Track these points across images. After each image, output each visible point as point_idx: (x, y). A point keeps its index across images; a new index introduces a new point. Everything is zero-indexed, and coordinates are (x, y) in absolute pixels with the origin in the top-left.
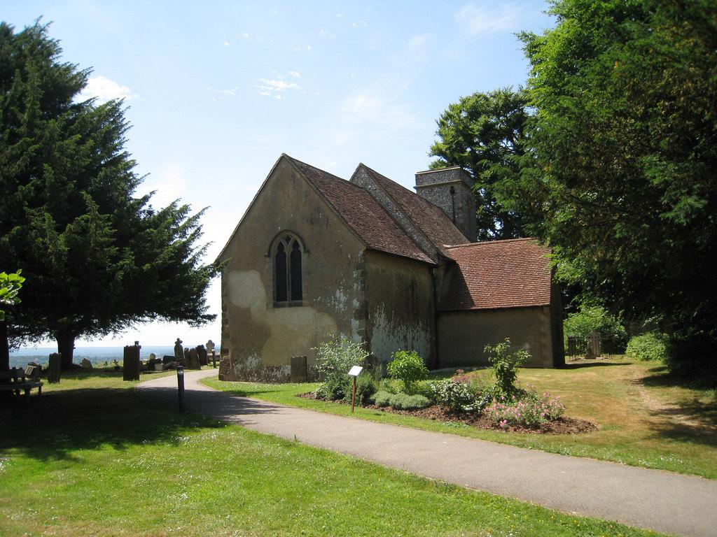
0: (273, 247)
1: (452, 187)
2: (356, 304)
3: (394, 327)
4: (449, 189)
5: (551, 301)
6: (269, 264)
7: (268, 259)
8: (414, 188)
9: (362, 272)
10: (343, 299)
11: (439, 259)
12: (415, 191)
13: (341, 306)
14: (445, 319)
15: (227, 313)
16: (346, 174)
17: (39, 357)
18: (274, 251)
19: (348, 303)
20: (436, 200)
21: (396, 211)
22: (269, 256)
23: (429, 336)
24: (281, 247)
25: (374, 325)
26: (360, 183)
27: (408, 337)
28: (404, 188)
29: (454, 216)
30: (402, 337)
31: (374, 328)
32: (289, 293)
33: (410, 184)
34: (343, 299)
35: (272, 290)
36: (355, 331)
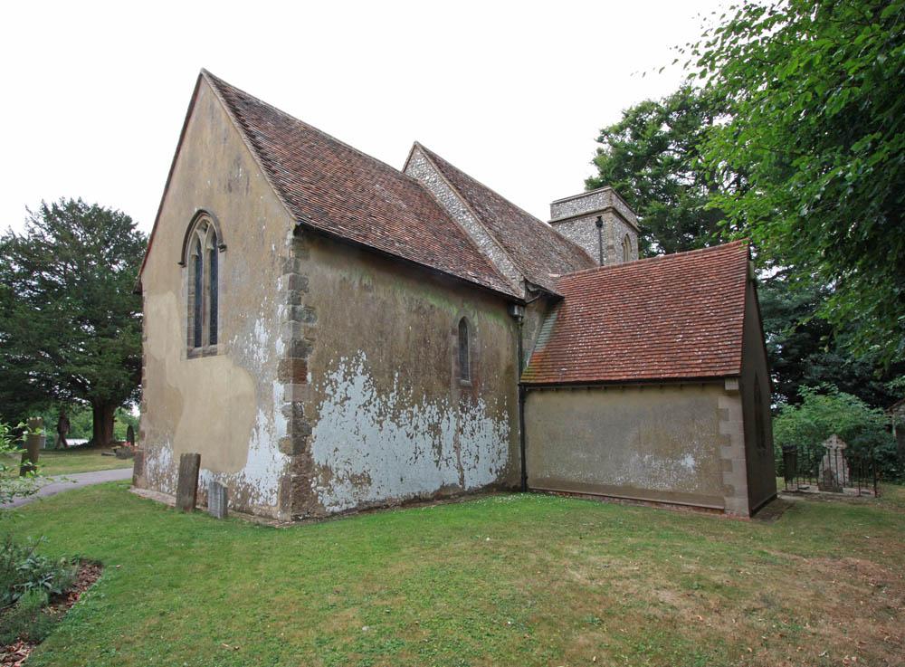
1: (599, 218)
2: (281, 348)
3: (400, 406)
4: (595, 219)
7: (184, 270)
10: (263, 338)
11: (528, 290)
13: (261, 352)
14: (536, 400)
16: (396, 159)
19: (270, 346)
20: (578, 238)
21: (464, 213)
23: (504, 427)
25: (321, 397)
26: (413, 173)
27: (444, 426)
29: (602, 260)
30: (423, 427)
33: (544, 216)
35: (186, 314)
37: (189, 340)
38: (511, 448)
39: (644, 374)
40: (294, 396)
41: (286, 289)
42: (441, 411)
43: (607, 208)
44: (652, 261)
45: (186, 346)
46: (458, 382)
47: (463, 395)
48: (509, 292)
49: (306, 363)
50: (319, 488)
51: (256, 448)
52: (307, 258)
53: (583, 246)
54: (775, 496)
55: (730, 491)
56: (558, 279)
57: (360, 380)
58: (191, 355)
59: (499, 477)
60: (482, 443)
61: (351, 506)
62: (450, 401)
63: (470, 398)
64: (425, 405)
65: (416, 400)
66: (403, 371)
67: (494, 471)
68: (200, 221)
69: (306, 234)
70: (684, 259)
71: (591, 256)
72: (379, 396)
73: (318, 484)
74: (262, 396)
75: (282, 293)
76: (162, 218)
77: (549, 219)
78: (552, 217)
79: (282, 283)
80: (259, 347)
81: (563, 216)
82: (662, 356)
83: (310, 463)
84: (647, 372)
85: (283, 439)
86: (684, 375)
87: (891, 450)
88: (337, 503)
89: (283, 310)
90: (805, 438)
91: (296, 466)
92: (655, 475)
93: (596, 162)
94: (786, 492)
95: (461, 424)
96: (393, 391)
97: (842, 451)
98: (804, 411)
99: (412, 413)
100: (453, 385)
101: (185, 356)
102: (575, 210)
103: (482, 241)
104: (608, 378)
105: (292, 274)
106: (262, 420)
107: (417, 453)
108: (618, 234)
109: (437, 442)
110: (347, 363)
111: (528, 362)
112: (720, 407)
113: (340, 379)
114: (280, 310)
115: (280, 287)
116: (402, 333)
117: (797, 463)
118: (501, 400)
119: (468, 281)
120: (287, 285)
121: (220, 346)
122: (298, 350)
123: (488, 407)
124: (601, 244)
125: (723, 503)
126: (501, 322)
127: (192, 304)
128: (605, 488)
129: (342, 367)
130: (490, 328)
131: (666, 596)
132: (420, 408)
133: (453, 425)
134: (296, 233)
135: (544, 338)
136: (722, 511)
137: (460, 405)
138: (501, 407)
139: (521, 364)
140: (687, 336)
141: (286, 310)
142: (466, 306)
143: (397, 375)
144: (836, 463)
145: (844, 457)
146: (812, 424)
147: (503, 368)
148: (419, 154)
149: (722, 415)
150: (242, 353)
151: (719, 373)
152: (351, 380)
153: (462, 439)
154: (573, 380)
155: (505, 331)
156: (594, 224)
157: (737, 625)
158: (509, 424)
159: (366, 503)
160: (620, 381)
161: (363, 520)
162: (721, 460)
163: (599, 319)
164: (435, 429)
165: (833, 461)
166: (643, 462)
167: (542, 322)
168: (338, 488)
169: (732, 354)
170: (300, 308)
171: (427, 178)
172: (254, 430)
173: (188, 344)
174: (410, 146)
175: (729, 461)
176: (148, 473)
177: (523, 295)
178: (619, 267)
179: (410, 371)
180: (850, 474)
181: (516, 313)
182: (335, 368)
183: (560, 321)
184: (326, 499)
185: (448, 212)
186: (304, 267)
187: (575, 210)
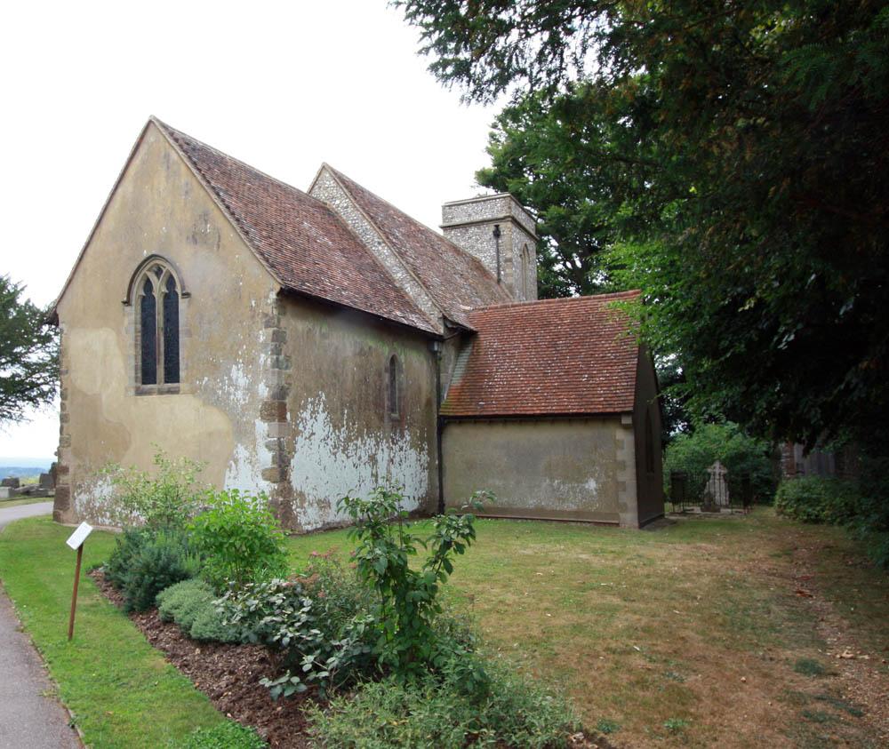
0: (135, 289)
1: (497, 226)
2: (264, 391)
3: (348, 439)
4: (492, 228)
5: (635, 407)
6: (132, 316)
7: (128, 309)
8: (442, 227)
9: (274, 333)
10: (243, 381)
11: (446, 326)
12: (441, 232)
13: (240, 394)
15: (66, 402)
16: (301, 181)
17: (14, 468)
18: (138, 291)
19: (250, 389)
20: (472, 247)
21: (379, 243)
22: (127, 303)
23: (425, 458)
24: (148, 285)
25: (296, 433)
26: (322, 195)
27: (379, 457)
28: (408, 221)
29: (499, 274)
30: (365, 458)
31: (299, 439)
32: (161, 372)
33: (432, 220)
34: (243, 381)
35: (133, 362)
36: (261, 442)
37: (136, 378)
38: (430, 478)
39: (554, 409)
40: (280, 433)
41: (269, 342)
42: (377, 443)
43: (505, 217)
44: (561, 301)
45: (134, 384)
46: (390, 417)
47: (393, 428)
48: (429, 329)
49: (286, 405)
50: (298, 510)
51: (235, 478)
52: (285, 314)
53: (479, 256)
54: (662, 516)
55: (624, 508)
56: (469, 311)
57: (322, 416)
58: (139, 392)
59: (421, 504)
60: (408, 472)
61: (319, 526)
62: (384, 433)
63: (398, 431)
64: (366, 438)
65: (360, 434)
66: (351, 408)
67: (416, 498)
68: (152, 264)
69: (294, 299)
70: (589, 302)
71: (487, 268)
72: (334, 431)
73: (297, 507)
74: (242, 432)
75: (265, 345)
76: (90, 251)
77: (441, 223)
78: (444, 221)
79: (263, 335)
80: (236, 389)
81: (457, 221)
82: (571, 393)
83: (291, 489)
84: (558, 408)
85: (267, 470)
86: (589, 411)
87: (766, 474)
88: (309, 523)
89: (265, 359)
90: (696, 465)
91: (282, 491)
92: (564, 497)
93: (490, 151)
94: (673, 513)
95: (392, 455)
96: (343, 426)
97: (724, 475)
98: (695, 439)
99: (356, 445)
100: (386, 420)
101: (132, 392)
102: (470, 215)
103: (399, 275)
104: (523, 412)
105: (275, 329)
106: (242, 452)
107: (361, 481)
108: (516, 245)
109: (374, 472)
110: (312, 403)
111: (445, 395)
112: (617, 438)
113: (308, 417)
114: (262, 359)
115: (262, 339)
116: (350, 374)
117: (687, 488)
118: (422, 431)
119: (397, 322)
120: (270, 338)
121: (182, 385)
122: (280, 394)
123: (412, 438)
124: (498, 256)
125: (619, 518)
126: (422, 358)
127: (139, 342)
128: (519, 511)
129: (309, 406)
130: (414, 363)
131: (584, 556)
132: (362, 441)
133: (386, 457)
134: (278, 294)
135: (459, 372)
136: (618, 525)
137: (392, 437)
138: (422, 439)
139: (439, 397)
140: (591, 376)
141: (269, 360)
142: (395, 345)
143: (346, 412)
144: (718, 489)
145: (725, 480)
146: (701, 451)
147: (424, 401)
148: (328, 175)
149: (618, 445)
150: (215, 393)
151: (617, 410)
152: (315, 418)
153: (393, 469)
154: (491, 413)
155: (425, 366)
156: (491, 233)
157: (577, 12)
158: (429, 454)
159: (328, 523)
160: (534, 415)
161: (329, 536)
162: (618, 483)
163: (513, 356)
164: (373, 459)
165: (717, 485)
166: (552, 486)
167: (458, 356)
168: (310, 511)
169: (628, 394)
170: (282, 357)
171: (338, 202)
172: (232, 462)
173: (136, 381)
174: (319, 167)
175: (624, 483)
176: (78, 508)
177: (441, 331)
178: (529, 304)
179: (355, 407)
180: (731, 496)
181: (436, 349)
182: (305, 408)
183: (475, 357)
184: (302, 519)
185: (361, 241)
186: (283, 323)
187: (470, 215)
